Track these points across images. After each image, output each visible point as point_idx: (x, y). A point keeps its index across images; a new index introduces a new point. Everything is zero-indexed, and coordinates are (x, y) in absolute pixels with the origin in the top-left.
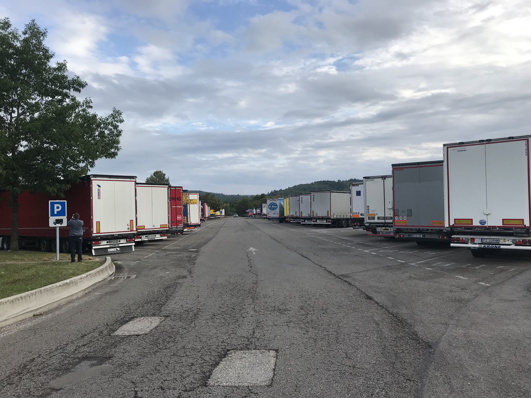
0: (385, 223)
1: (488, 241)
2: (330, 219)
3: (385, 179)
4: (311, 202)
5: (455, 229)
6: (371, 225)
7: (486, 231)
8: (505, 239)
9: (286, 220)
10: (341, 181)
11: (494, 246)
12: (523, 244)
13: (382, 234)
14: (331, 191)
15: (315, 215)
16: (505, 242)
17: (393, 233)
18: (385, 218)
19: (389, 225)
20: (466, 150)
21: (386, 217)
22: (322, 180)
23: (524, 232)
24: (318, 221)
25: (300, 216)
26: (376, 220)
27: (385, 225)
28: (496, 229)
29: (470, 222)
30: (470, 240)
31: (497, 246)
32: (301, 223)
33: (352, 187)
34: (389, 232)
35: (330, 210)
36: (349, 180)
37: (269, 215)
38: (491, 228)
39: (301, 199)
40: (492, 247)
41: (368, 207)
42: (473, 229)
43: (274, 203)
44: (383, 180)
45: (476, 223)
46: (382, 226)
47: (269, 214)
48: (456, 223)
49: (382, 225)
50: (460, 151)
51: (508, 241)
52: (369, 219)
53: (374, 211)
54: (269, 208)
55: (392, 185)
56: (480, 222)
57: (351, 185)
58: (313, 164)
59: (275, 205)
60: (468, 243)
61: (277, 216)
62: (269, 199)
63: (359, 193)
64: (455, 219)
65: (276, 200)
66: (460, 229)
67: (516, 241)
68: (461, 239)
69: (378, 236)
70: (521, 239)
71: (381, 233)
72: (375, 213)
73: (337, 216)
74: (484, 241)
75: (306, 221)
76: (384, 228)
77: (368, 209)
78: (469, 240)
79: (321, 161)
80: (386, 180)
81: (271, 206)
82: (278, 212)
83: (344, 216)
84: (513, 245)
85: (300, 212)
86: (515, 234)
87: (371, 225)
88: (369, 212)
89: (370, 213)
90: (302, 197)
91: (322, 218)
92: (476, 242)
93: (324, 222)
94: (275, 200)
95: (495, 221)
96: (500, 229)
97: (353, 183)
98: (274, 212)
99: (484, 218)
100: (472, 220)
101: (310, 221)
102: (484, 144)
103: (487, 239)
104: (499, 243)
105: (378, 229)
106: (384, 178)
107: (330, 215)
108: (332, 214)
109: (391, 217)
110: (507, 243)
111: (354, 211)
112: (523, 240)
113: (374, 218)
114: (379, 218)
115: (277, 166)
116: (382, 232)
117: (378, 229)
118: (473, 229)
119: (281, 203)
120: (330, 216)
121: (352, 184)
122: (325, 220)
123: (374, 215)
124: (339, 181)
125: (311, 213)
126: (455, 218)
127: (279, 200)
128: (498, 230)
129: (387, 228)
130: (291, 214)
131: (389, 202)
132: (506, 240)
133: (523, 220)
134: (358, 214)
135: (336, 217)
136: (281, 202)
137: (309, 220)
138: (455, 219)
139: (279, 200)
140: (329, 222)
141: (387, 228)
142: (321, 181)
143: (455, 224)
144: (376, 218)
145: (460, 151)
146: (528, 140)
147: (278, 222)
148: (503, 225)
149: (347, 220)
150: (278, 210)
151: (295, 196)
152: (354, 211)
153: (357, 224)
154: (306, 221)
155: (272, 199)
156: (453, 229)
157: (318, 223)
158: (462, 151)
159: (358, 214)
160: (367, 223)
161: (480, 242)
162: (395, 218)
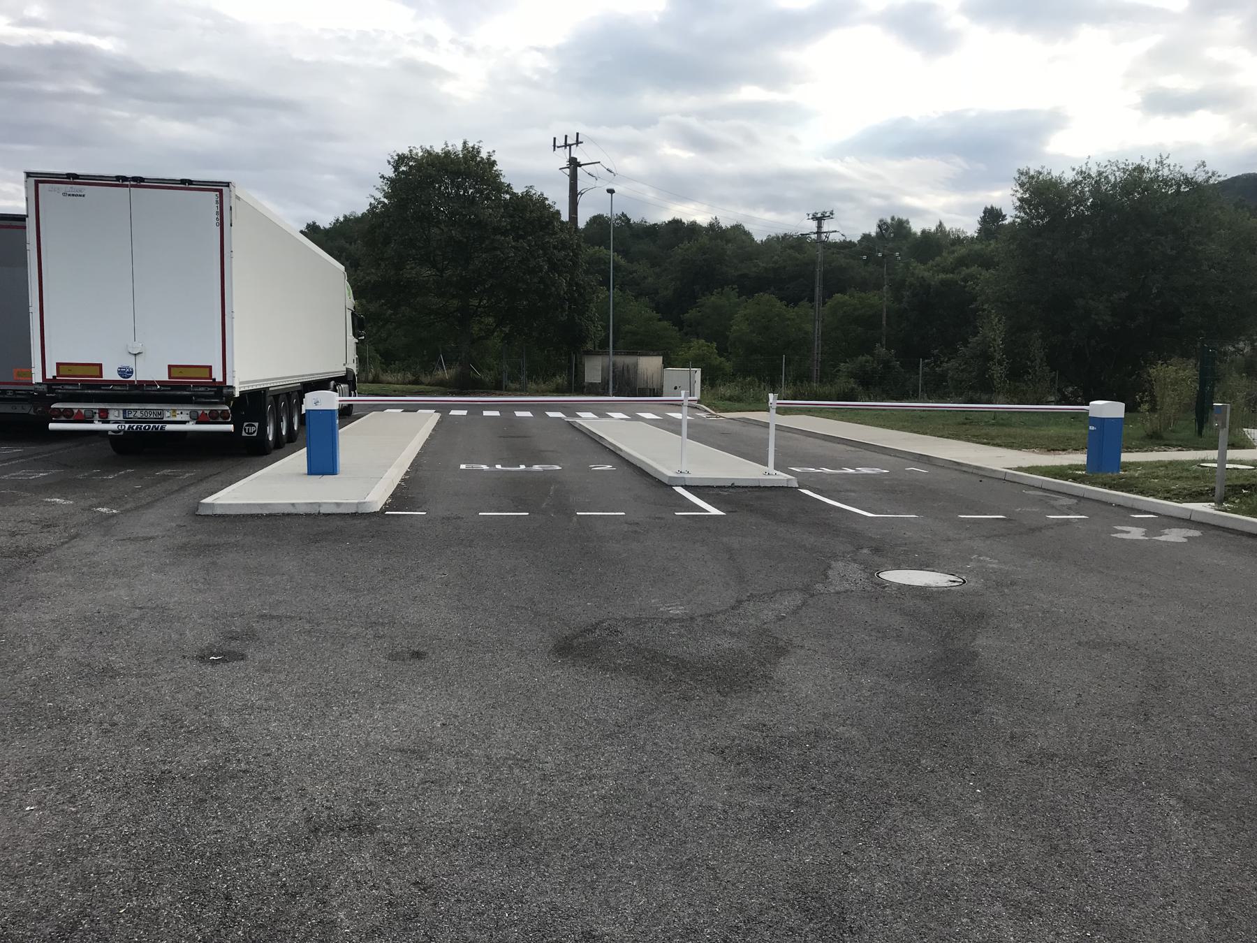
1: (139, 414)
8: (174, 411)
11: (152, 425)
12: (211, 420)
23: (213, 393)
29: (205, 373)
40: (147, 428)
45: (110, 374)
50: (69, 195)
51: (182, 413)
56: (118, 371)
60: (92, 422)
64: (58, 365)
68: (76, 411)
70: (200, 409)
74: (131, 416)
78: (95, 413)
84: (191, 423)
92: (111, 417)
95: (152, 371)
96: (162, 388)
99: (129, 362)
100: (100, 365)
102: (127, 186)
110: (178, 418)
118: (103, 388)
128: (159, 390)
145: (69, 195)
146: (221, 192)
158: (73, 195)
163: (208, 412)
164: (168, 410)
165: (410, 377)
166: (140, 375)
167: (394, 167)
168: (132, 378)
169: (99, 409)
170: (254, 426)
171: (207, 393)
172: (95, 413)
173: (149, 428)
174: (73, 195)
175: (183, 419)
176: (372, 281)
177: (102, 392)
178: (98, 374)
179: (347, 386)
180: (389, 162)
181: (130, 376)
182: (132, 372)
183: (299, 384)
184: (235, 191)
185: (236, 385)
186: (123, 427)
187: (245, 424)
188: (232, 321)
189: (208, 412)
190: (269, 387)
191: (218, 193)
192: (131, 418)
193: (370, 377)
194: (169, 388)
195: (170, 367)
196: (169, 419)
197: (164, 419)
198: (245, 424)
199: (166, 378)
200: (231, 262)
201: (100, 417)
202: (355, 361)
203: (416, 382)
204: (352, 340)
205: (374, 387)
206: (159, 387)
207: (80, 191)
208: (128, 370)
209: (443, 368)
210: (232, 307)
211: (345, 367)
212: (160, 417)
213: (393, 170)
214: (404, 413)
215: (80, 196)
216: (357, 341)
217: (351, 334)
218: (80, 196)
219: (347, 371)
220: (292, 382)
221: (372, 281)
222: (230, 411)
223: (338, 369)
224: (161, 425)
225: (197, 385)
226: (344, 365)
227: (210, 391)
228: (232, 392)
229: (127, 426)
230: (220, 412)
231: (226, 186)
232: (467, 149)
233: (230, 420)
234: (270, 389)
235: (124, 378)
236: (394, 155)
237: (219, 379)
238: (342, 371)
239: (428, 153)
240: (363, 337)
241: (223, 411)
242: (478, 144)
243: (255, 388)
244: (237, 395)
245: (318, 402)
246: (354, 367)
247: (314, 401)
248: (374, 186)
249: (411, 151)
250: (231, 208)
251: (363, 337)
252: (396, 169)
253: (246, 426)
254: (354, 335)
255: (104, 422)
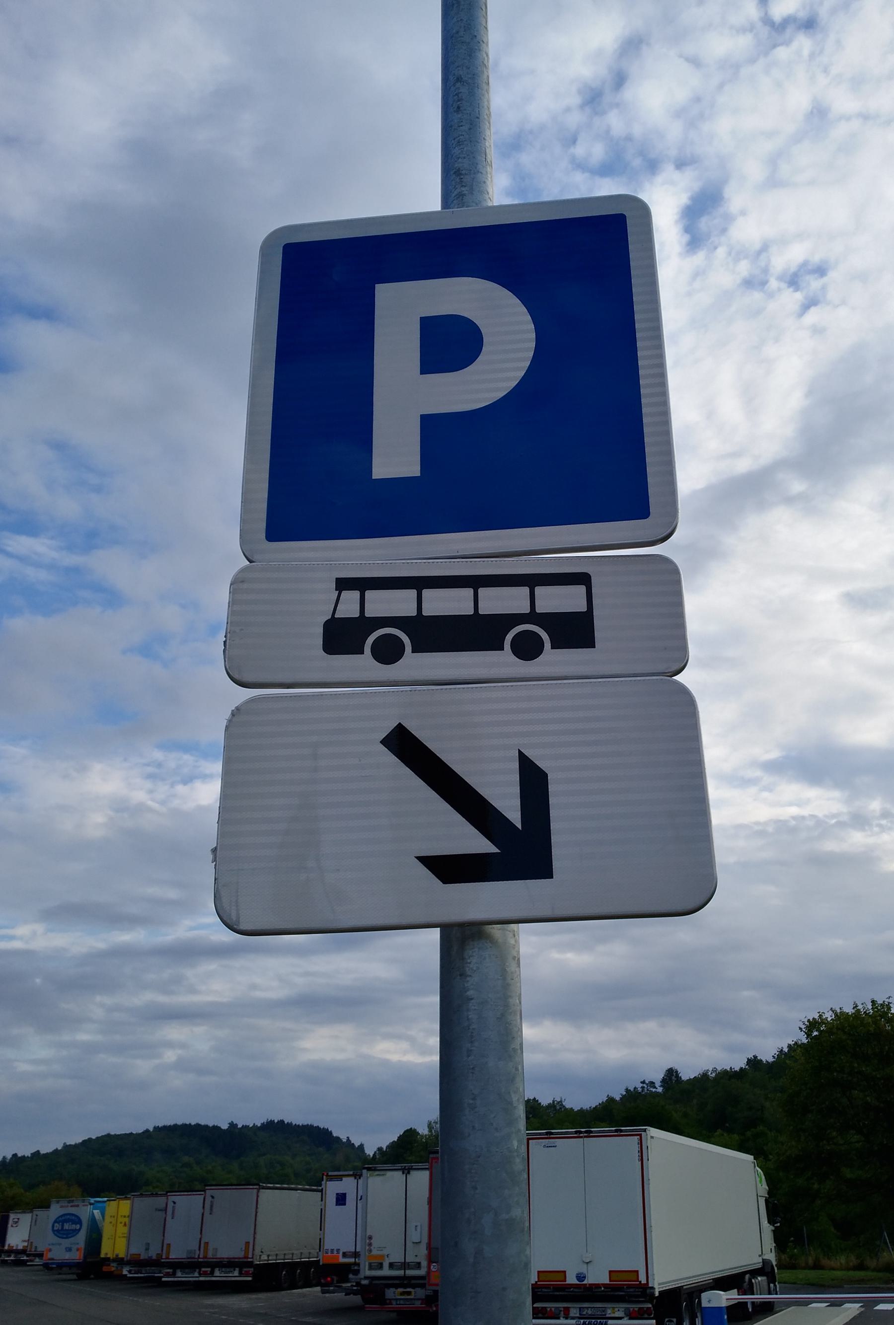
0: (405, 1277)
1: (590, 1312)
2: (250, 1264)
3: (409, 1173)
4: (203, 1214)
5: (540, 1290)
6: (374, 1282)
7: (585, 1293)
8: (613, 1308)
9: (105, 1269)
10: (240, 1126)
11: (599, 1321)
12: (639, 1316)
13: (397, 1304)
14: (259, 1185)
15: (210, 1255)
16: (614, 1313)
17: (420, 1302)
18: (405, 1265)
19: (413, 1282)
20: (556, 1146)
21: (409, 1263)
22: (180, 1123)
23: (639, 1293)
24: (217, 1272)
25: (199, 1255)
26: (386, 1272)
27: (405, 1282)
28: (600, 1290)
29: (633, 1277)
30: (562, 1313)
31: (602, 1321)
32: (164, 1279)
33: (327, 1182)
34: (411, 1299)
35: (254, 1238)
36: (263, 1124)
37: (50, 1255)
38: (625, 1287)
39: (172, 1204)
40: (595, 1323)
41: (370, 1238)
42: (567, 1290)
43: (73, 1215)
44: (405, 1175)
45: (571, 1279)
46: (396, 1286)
47: (50, 1250)
48: (541, 1279)
49: (398, 1282)
50: (547, 1147)
51: (619, 1310)
52: (371, 1267)
53: (380, 1249)
54: (53, 1230)
55: (427, 1195)
56: (577, 1277)
57: (325, 1177)
58: (143, 1067)
59: (74, 1222)
60: (558, 1318)
61: (76, 1256)
62: (58, 1202)
63: (341, 1199)
64: (539, 1272)
65: (81, 1204)
66: (546, 1290)
67: (630, 1310)
68: (549, 1309)
69: (388, 1311)
70: (636, 1306)
71: (394, 1302)
72: (385, 1252)
73: (268, 1256)
74: (585, 1313)
75: (179, 1274)
76: (401, 1290)
77: (370, 1245)
78: (561, 1311)
79: (170, 1056)
80: (410, 1175)
81: (63, 1226)
82: (82, 1245)
83: (270, 1258)
84: (625, 1319)
85: (202, 1246)
86: (627, 1298)
87: (374, 1282)
88: (370, 1251)
89: (375, 1252)
90: (176, 1199)
91: (230, 1264)
92: (571, 1315)
93: (234, 1275)
94: (78, 1206)
95: (598, 1276)
96: (606, 1290)
97: (330, 1173)
98: (66, 1242)
99: (583, 1269)
100: (564, 1272)
101: (229, 1272)
102: (581, 1137)
103: (588, 1308)
104: (606, 1315)
105: (390, 1293)
106: (406, 1171)
107: (253, 1254)
108: (257, 1251)
109: (417, 1263)
110: (617, 1315)
111: (328, 1245)
112: (640, 1309)
113: (380, 1267)
114: (392, 1266)
115: (23, 1067)
116: (397, 1300)
117: (390, 1293)
118: (567, 1290)
119: (93, 1214)
120: (252, 1258)
121: (327, 1175)
122: (237, 1269)
123: (382, 1257)
124: (232, 1125)
125: (199, 1250)
126: (539, 1270)
127: (91, 1204)
128: (603, 1291)
129: (408, 1290)
130: (134, 1251)
131: (416, 1226)
132: (616, 1309)
133: (637, 1272)
134: (335, 1252)
135: (266, 1258)
136: (96, 1212)
137: (187, 1271)
138: (539, 1272)
139: (91, 1204)
140: (247, 1274)
141: (408, 1290)
142: (175, 1126)
143: (539, 1281)
144: (386, 1265)
145: (547, 1147)
146: (640, 1135)
147: (75, 1277)
148: (610, 1282)
149: (292, 1266)
150: (81, 1239)
151: (152, 1194)
152: (328, 1245)
153: (332, 1280)
154: (179, 1274)
155: (69, 1202)
156: (536, 1290)
157: (180, 1279)
158: (550, 1147)
159: (335, 1252)
160: (366, 1278)
161: (578, 1315)
162: (432, 1267)
163: (636, 1309)
164: (609, 1308)
165: (854, 1261)
166: (590, 1280)
167: (806, 1033)
168: (585, 1282)
169: (564, 1307)
170: (673, 1321)
171: (636, 1293)
172: (561, 1311)
173: (597, 1323)
174: (550, 1147)
175: (620, 1316)
176: (793, 1156)
177: (566, 1293)
178: (563, 1279)
179: (764, 1278)
180: (800, 1029)
181: (583, 1281)
182: (585, 1277)
183: (711, 1281)
184: (650, 1134)
185: (656, 1286)
186: (579, 1322)
187: (666, 1320)
188: (651, 1233)
189: (636, 1309)
190: (682, 1286)
191: (639, 1137)
192: (584, 1315)
193: (810, 1261)
194: (609, 1290)
195: (610, 1272)
196: (609, 1316)
197: (607, 1316)
198: (666, 1320)
199: (607, 1281)
200: (649, 1188)
201: (564, 1314)
202: (773, 1250)
203: (861, 1267)
204: (768, 1228)
205: (812, 1275)
206: (603, 1289)
207: (554, 1143)
208: (582, 1276)
209: (888, 1248)
210: (653, 1271)
211: (761, 1258)
212: (604, 1314)
213: (806, 1036)
214: (831, 1308)
215: (554, 1146)
216: (773, 1228)
217: (766, 1222)
218: (554, 1146)
219: (763, 1262)
220: (694, 1282)
221: (793, 1156)
222: (652, 1309)
223: (752, 1260)
224: (605, 1321)
225: (629, 1286)
226: (760, 1256)
227: (638, 1292)
228: (653, 1292)
229: (582, 1321)
230: (645, 1309)
231: (644, 1131)
232: (877, 1008)
233: (652, 1316)
234: (685, 1287)
235: (580, 1282)
236: (806, 1020)
237: (644, 1281)
238: (759, 1263)
239: (840, 1016)
240: (779, 1224)
241: (648, 1308)
242: (887, 1000)
243: (671, 1287)
244: (657, 1294)
245: (710, 1301)
246: (772, 1257)
247: (707, 1300)
248: (800, 1021)
249: (820, 1016)
250: (648, 1147)
251: (779, 1224)
252: (808, 1035)
253: (667, 1322)
254: (769, 1222)
255: (567, 1318)
